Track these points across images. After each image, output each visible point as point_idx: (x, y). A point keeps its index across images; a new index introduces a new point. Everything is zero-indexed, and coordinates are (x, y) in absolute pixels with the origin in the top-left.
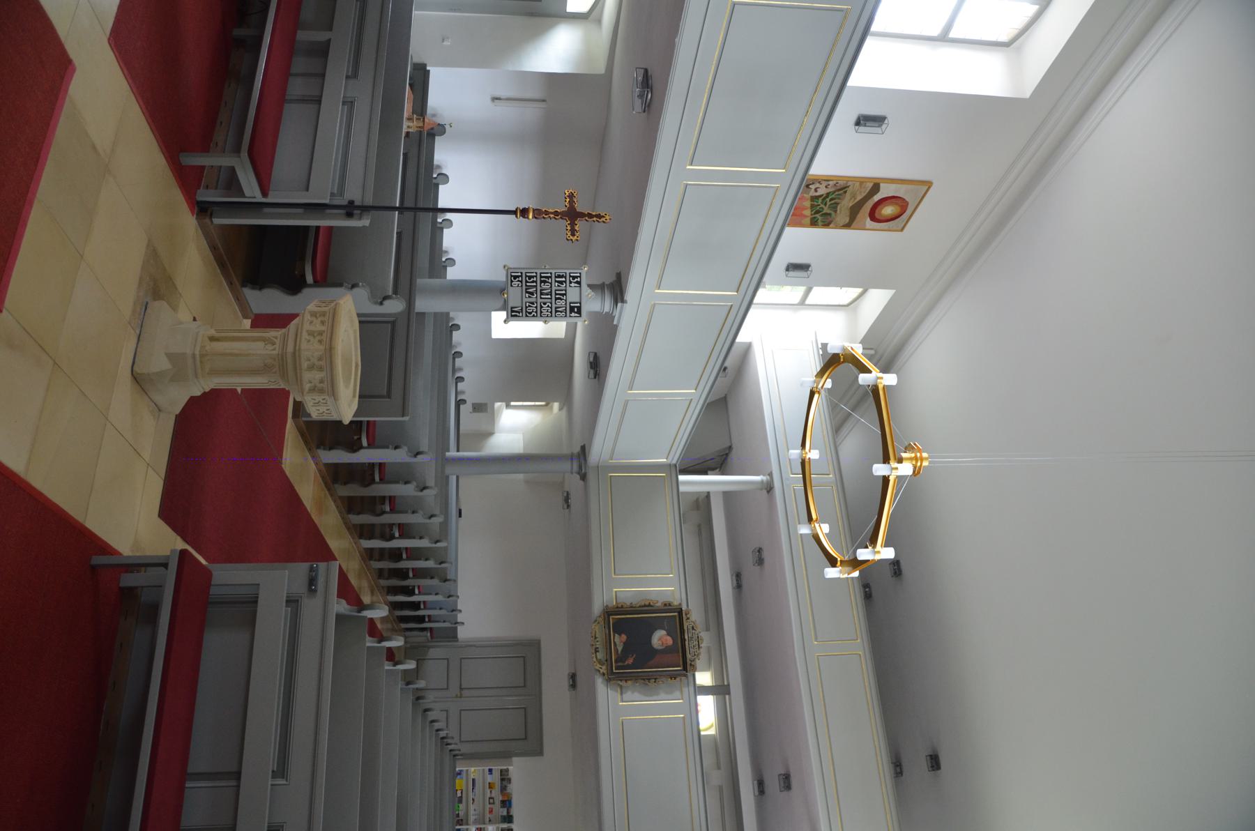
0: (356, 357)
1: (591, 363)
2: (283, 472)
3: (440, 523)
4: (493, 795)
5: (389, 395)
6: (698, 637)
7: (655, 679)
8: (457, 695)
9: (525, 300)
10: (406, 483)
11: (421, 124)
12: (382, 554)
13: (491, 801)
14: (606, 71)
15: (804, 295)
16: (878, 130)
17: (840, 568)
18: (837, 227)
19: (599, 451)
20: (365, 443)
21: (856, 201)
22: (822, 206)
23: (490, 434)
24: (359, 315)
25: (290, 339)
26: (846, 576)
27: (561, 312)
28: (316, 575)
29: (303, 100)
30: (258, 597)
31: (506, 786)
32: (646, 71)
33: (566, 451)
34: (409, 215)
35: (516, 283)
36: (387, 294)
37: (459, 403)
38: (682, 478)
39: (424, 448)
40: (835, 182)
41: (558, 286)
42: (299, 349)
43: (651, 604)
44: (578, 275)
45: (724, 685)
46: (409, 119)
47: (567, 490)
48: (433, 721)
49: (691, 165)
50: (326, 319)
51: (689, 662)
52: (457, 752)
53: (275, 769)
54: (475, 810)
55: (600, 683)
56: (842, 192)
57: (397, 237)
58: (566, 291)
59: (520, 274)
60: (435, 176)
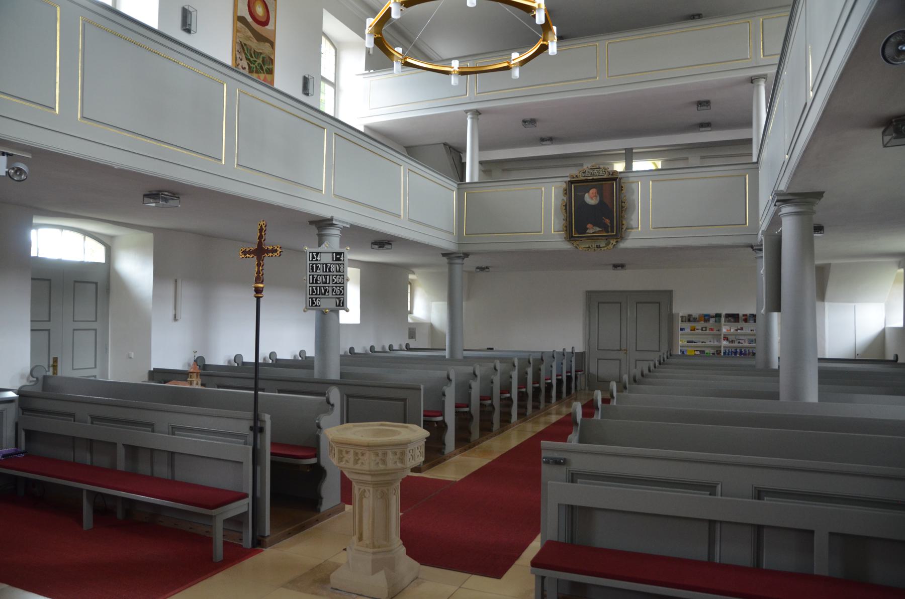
0: (375, 426)
1: (379, 247)
2: (462, 481)
3: (500, 363)
4: (700, 328)
5: (404, 400)
6: (591, 169)
7: (622, 202)
8: (625, 353)
9: (330, 296)
10: (470, 388)
11: (195, 375)
12: (522, 406)
13: (704, 329)
14: (151, 232)
15: (328, 84)
16: (194, 14)
17: (549, 41)
18: (274, 54)
19: (447, 243)
20: (440, 419)
21: (252, 36)
22: (256, 64)
23: (431, 326)
24: (342, 423)
25: (361, 478)
26: (556, 37)
27: (340, 268)
28: (551, 459)
29: (172, 465)
30: (568, 505)
31: (694, 318)
32: (145, 196)
33: (446, 270)
34: (261, 384)
35: (317, 303)
36: (325, 401)
37: (408, 348)
38: (468, 180)
39: (444, 374)
40: (237, 53)
41: (320, 270)
42: (369, 471)
43: (564, 204)
44: (311, 254)
45: (625, 153)
46: (191, 384)
47: (475, 269)
48: (649, 371)
49: (221, 160)
50: (344, 450)
51: (610, 176)
52: (669, 354)
53: (709, 493)
54: (710, 341)
55: (624, 245)
56: (245, 48)
57: (282, 393)
58: (323, 264)
59: (310, 299)
60: (236, 365)
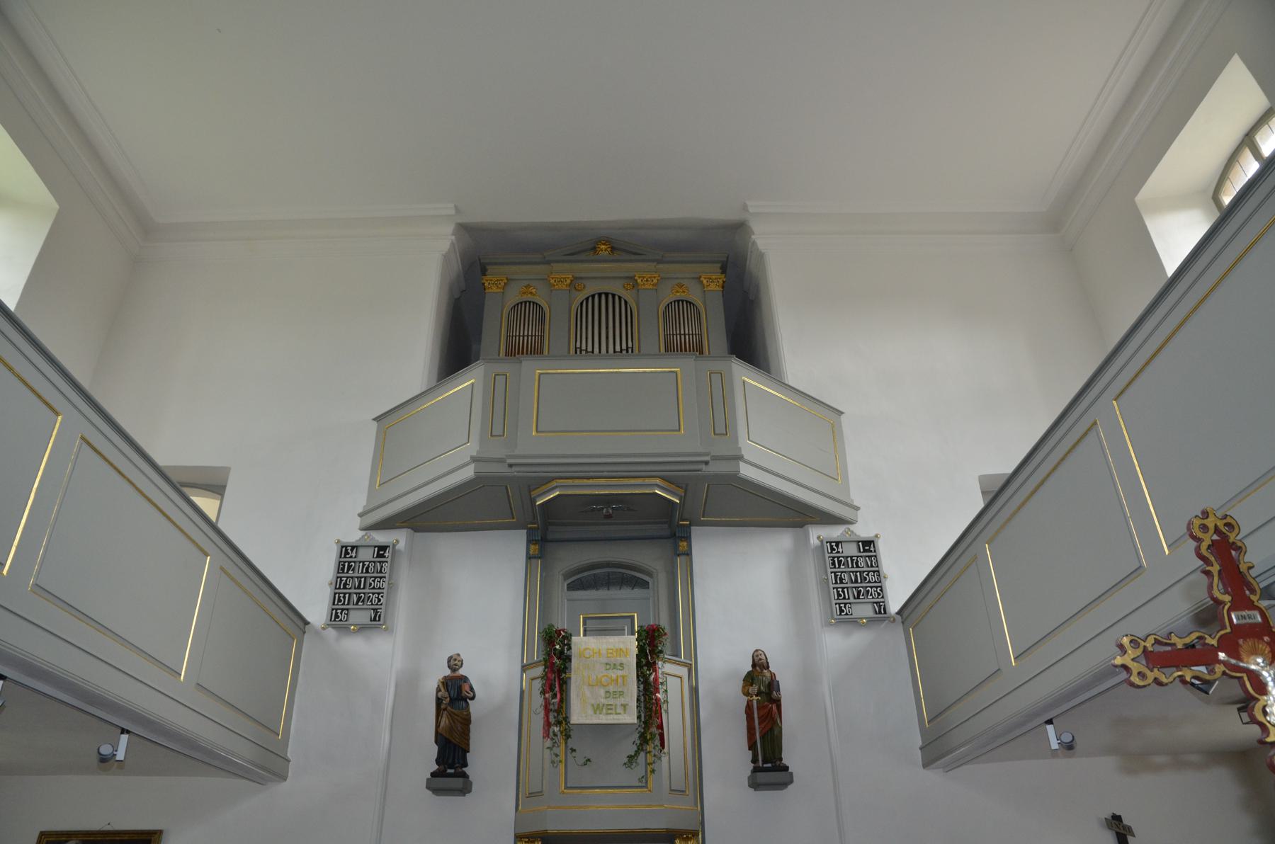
27: (872, 561)
58: (847, 557)
